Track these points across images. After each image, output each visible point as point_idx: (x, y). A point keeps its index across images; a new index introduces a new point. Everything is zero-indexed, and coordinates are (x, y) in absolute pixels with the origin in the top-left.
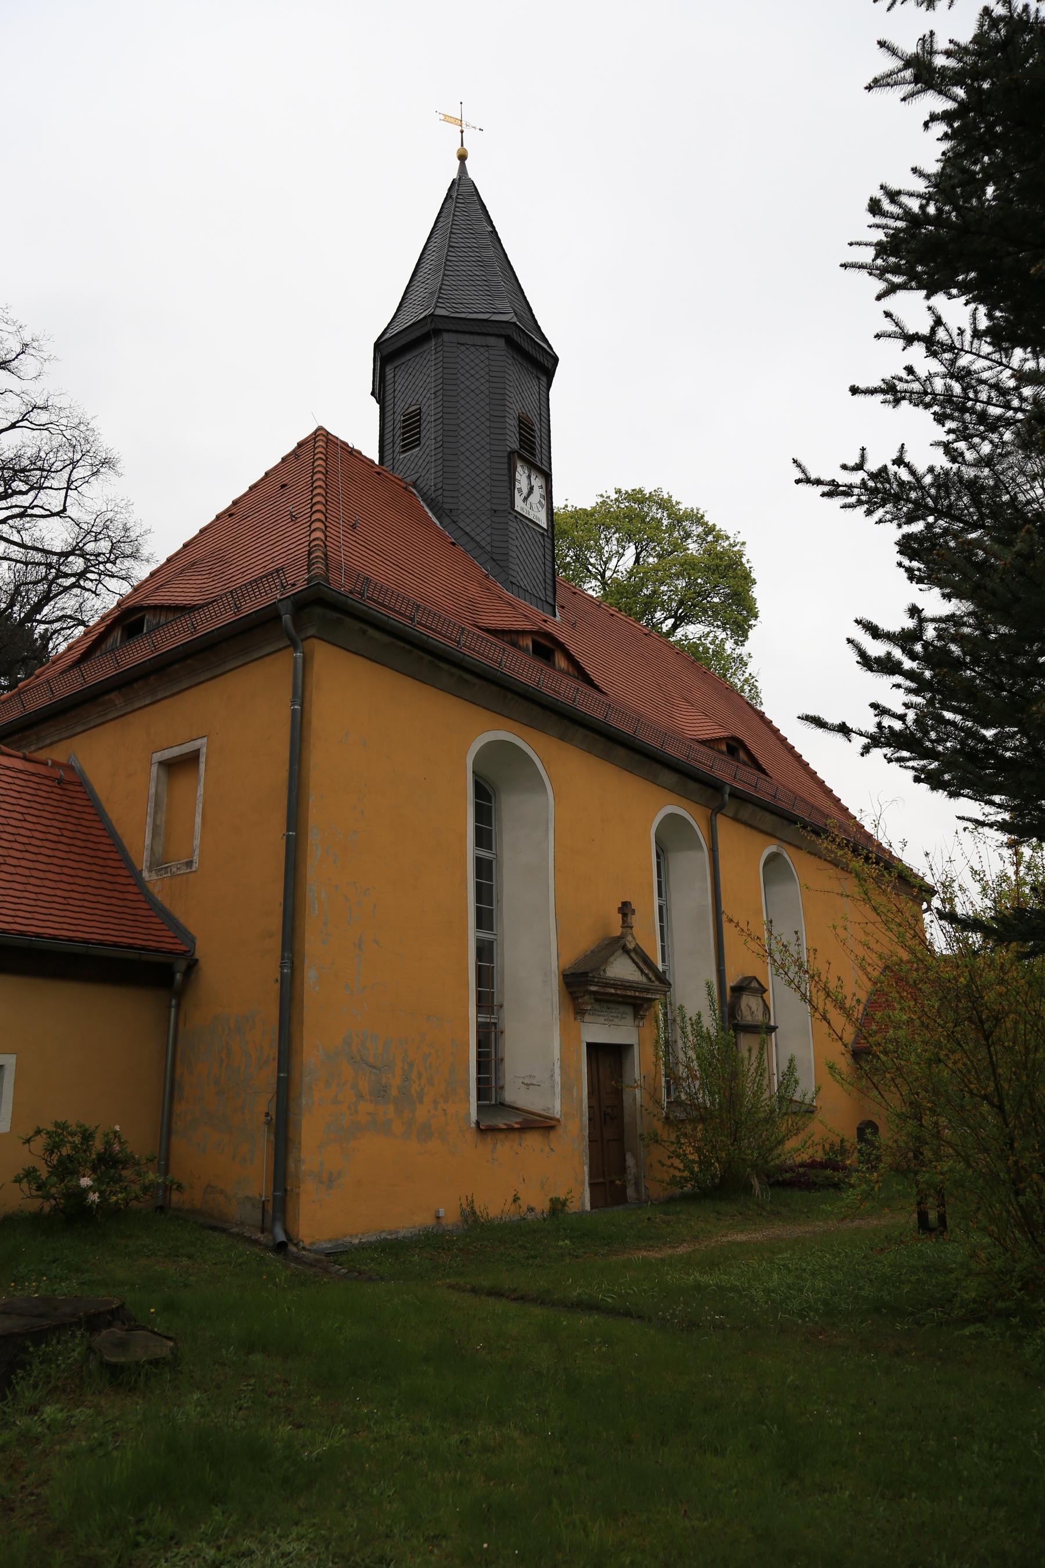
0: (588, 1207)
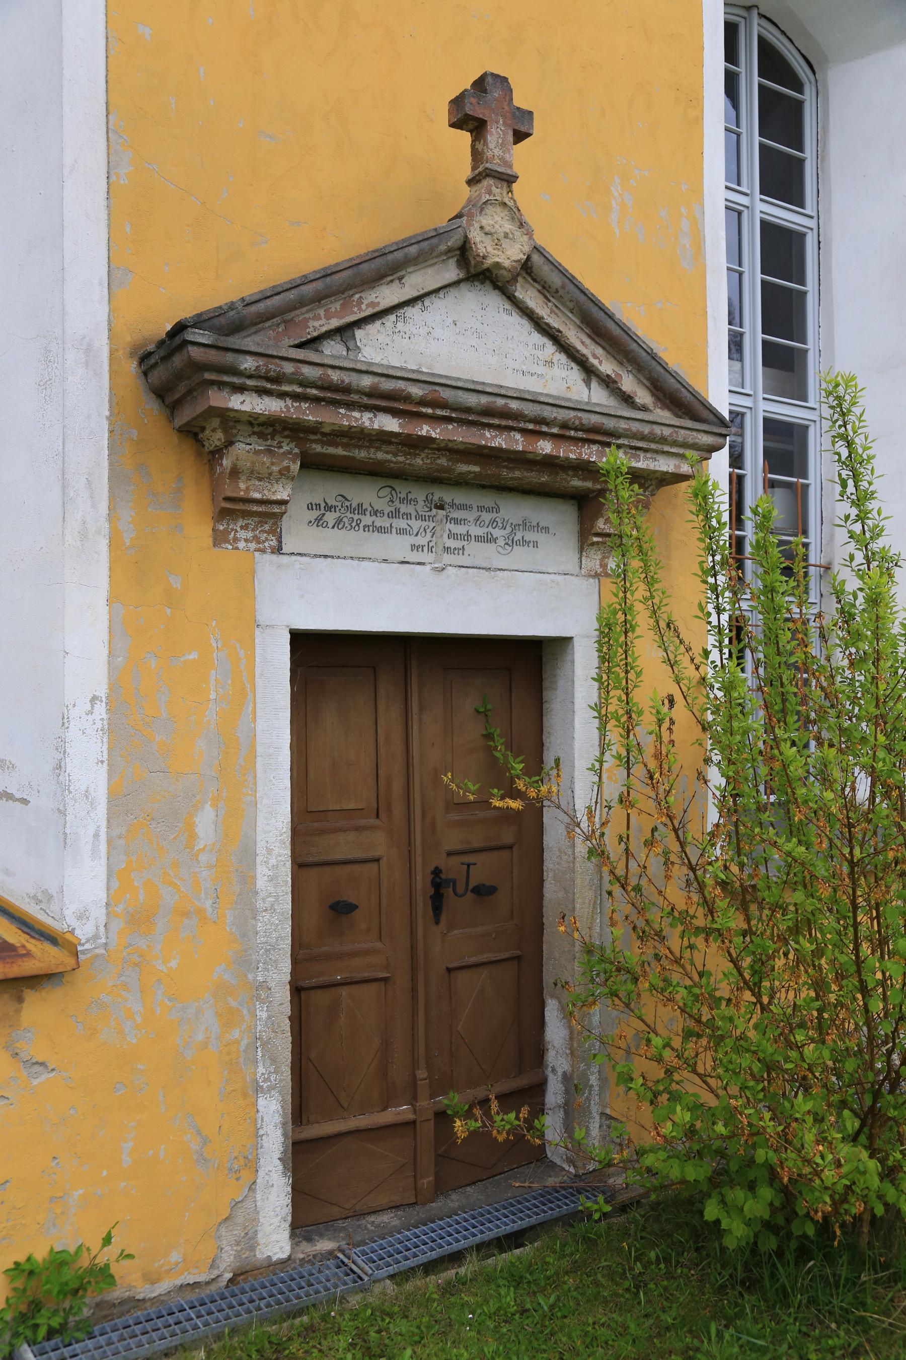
0: (275, 1241)
